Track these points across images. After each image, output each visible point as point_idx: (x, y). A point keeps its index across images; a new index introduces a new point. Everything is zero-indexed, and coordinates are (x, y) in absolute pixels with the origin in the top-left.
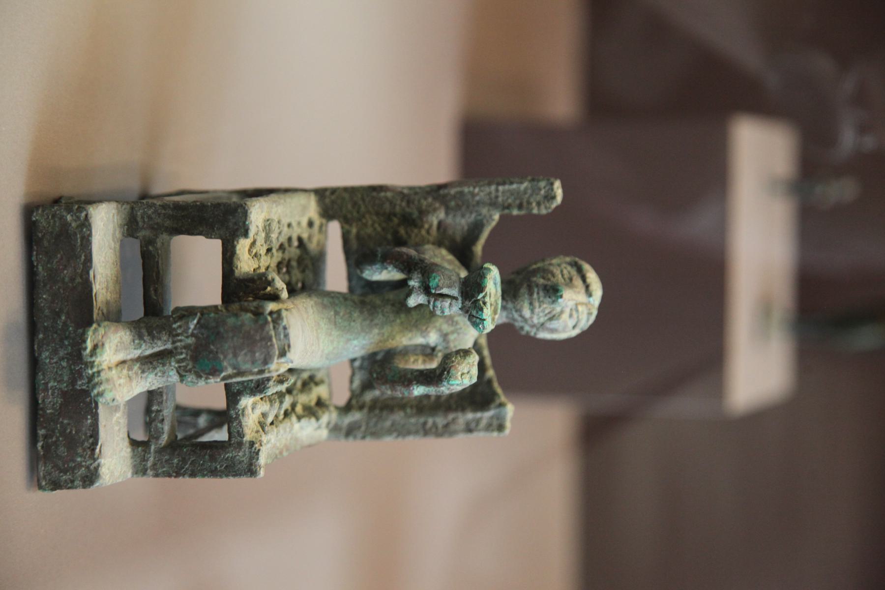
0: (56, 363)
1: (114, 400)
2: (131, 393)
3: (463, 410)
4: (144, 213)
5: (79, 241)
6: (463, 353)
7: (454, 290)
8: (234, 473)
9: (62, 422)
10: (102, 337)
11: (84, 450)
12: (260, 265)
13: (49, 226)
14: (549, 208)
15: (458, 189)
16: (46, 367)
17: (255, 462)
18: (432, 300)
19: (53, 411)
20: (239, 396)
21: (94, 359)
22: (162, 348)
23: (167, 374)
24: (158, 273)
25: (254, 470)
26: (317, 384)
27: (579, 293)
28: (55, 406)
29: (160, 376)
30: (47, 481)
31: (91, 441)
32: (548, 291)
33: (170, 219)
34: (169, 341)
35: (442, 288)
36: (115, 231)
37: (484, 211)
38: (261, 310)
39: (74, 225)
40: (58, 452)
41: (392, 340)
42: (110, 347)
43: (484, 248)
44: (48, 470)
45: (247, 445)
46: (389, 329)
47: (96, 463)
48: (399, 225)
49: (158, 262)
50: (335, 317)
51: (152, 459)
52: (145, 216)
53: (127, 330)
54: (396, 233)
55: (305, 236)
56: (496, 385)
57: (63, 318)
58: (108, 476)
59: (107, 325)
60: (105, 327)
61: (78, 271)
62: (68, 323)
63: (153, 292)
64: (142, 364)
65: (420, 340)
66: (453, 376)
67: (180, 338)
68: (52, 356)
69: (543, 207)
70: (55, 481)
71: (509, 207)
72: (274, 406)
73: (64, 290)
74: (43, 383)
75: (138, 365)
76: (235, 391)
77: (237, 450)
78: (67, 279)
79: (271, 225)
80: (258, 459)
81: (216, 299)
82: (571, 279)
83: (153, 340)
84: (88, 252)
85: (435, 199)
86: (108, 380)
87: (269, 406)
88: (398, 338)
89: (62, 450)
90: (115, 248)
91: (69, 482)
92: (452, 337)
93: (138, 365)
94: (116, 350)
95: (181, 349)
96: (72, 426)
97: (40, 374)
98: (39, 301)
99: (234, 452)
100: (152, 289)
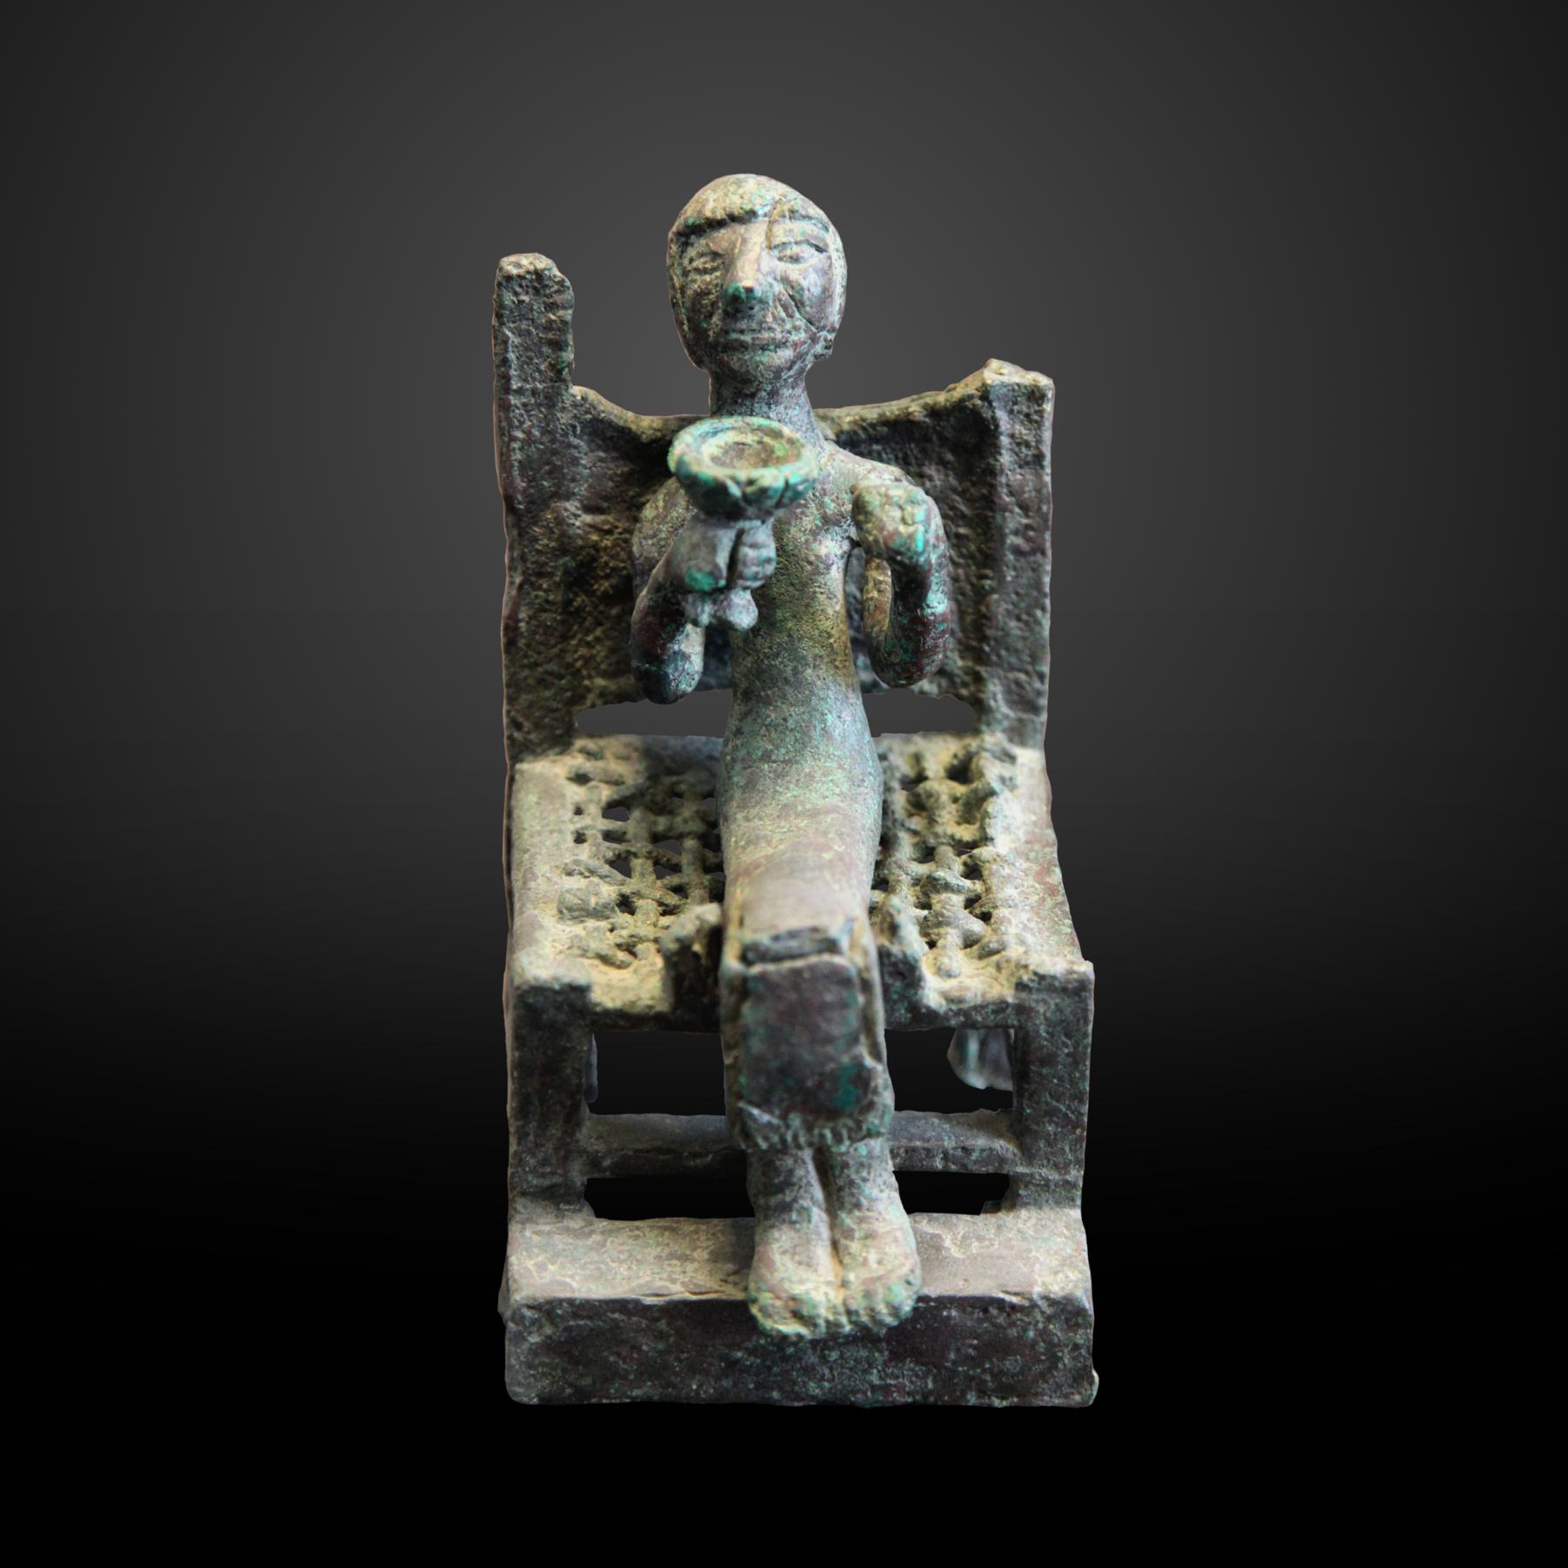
0: (831, 1369)
1: (909, 1283)
3: (992, 472)
4: (533, 1171)
5: (582, 1323)
6: (859, 513)
7: (720, 540)
8: (1082, 1021)
9: (954, 1363)
10: (778, 1298)
11: (1013, 1324)
12: (652, 937)
13: (550, 1374)
14: (561, 283)
15: (516, 473)
16: (840, 1387)
17: (1060, 982)
18: (740, 582)
19: (930, 1378)
20: (920, 1009)
21: (821, 1322)
22: (811, 1167)
23: (865, 1160)
25: (1075, 984)
27: (744, 241)
28: (920, 1373)
29: (869, 1173)
30: (1072, 1390)
31: (994, 1311)
32: (737, 311)
33: (548, 1126)
34: (797, 1154)
35: (716, 566)
36: (567, 1230)
37: (564, 418)
38: (737, 983)
39: (548, 1330)
41: (830, 636)
42: (801, 1282)
43: (640, 410)
45: (1024, 995)
46: (806, 644)
47: (1040, 1303)
48: (591, 593)
50: (774, 762)
51: (1044, 1172)
52: (541, 1170)
53: (769, 1235)
54: (606, 599)
55: (606, 793)
56: (941, 398)
57: (739, 1354)
58: (1070, 1274)
59: (756, 1283)
60: (759, 1290)
61: (644, 1326)
62: (750, 1346)
63: (698, 1161)
64: (842, 1206)
65: (835, 575)
66: (906, 544)
67: (789, 1138)
68: (818, 1376)
69: (558, 298)
70: (1074, 1378)
71: (557, 370)
72: (948, 917)
73: (683, 1352)
74: (873, 1392)
75: (843, 1215)
76: (909, 1015)
77: (1033, 1014)
78: (661, 1346)
79: (569, 905)
80: (1054, 978)
82: (715, 255)
83: (793, 1185)
84: (604, 1307)
85: (535, 521)
86: (868, 1295)
87: (949, 930)
88: (826, 625)
89: (1011, 1364)
90: (603, 1233)
91: (1076, 1353)
92: (831, 508)
93: (843, 1215)
94: (809, 1265)
96: (963, 1345)
97: (853, 1399)
98: (703, 1396)
99: (1038, 1022)
100: (692, 1163)
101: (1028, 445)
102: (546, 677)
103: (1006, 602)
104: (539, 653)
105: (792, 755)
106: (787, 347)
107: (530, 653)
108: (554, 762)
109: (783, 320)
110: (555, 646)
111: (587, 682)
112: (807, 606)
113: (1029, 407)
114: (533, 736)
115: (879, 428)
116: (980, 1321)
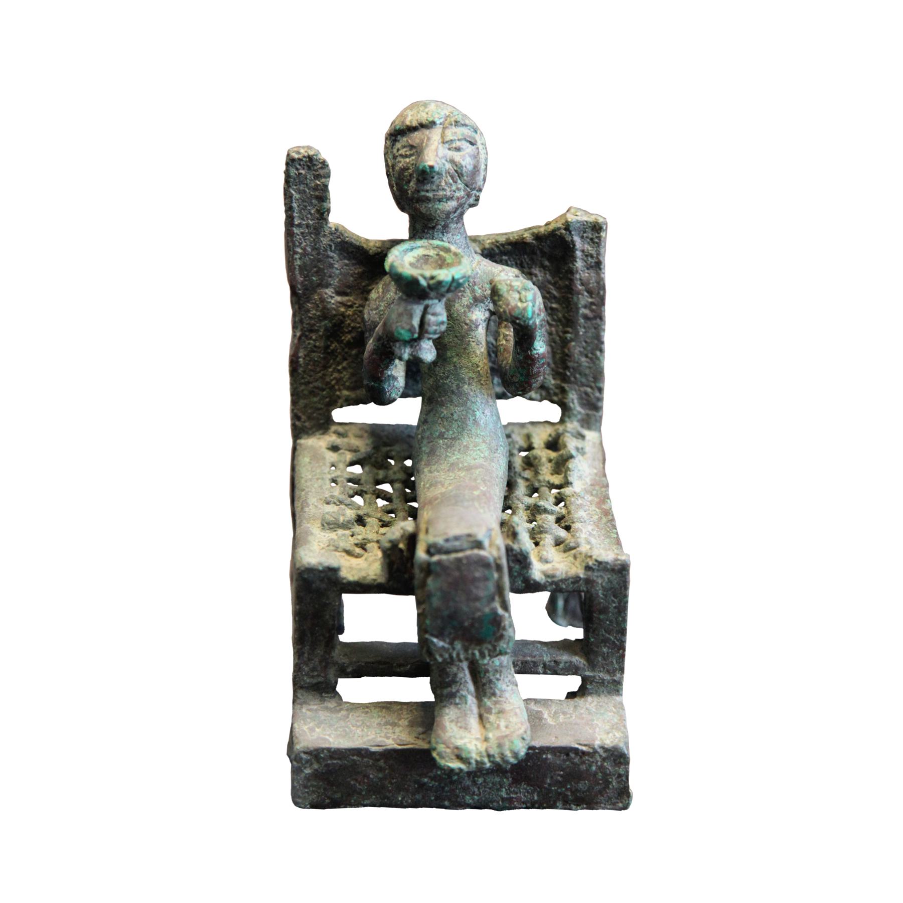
0: (479, 788)
1: (523, 739)
2: (518, 711)
3: (571, 272)
4: (307, 675)
5: (335, 762)
6: (495, 296)
7: (415, 311)
8: (623, 588)
9: (550, 785)
10: (448, 747)
11: (583, 763)
12: (375, 540)
13: (317, 792)
15: (297, 272)
17: (611, 566)
19: (536, 794)
20: (530, 581)
21: (473, 761)
22: (467, 672)
23: (498, 668)
25: (619, 567)
28: (530, 791)
29: (500, 676)
30: (618, 801)
31: (572, 755)
32: (425, 179)
33: (316, 648)
34: (459, 665)
35: (412, 326)
36: (327, 708)
37: (325, 241)
38: (425, 566)
39: (316, 766)
40: (585, 790)
41: (478, 366)
42: (461, 738)
45: (590, 573)
46: (464, 371)
47: (599, 750)
48: (340, 342)
49: (366, 663)
50: (446, 439)
51: (601, 675)
52: (311, 674)
53: (443, 711)
54: (349, 345)
57: (426, 780)
58: (616, 734)
59: (435, 739)
60: (437, 743)
61: (371, 763)
62: (432, 775)
64: (485, 695)
65: (481, 331)
67: (454, 655)
68: (471, 793)
70: (619, 794)
72: (546, 528)
73: (393, 779)
74: (502, 802)
75: (486, 700)
76: (523, 585)
78: (380, 775)
79: (328, 521)
80: (607, 563)
81: (410, 601)
82: (412, 147)
83: (457, 682)
84: (348, 753)
85: (308, 300)
86: (500, 746)
87: (547, 535)
88: (476, 360)
89: (582, 786)
91: (620, 779)
92: (479, 292)
93: (486, 700)
94: (466, 729)
96: (555, 774)
99: (598, 589)
100: (398, 670)
102: (314, 390)
103: (580, 347)
104: (311, 376)
105: (456, 435)
106: (453, 200)
108: (319, 439)
109: (451, 185)
110: (320, 372)
111: (338, 393)
112: (465, 349)
113: (592, 235)
114: (307, 424)
115: (506, 247)
116: (564, 761)
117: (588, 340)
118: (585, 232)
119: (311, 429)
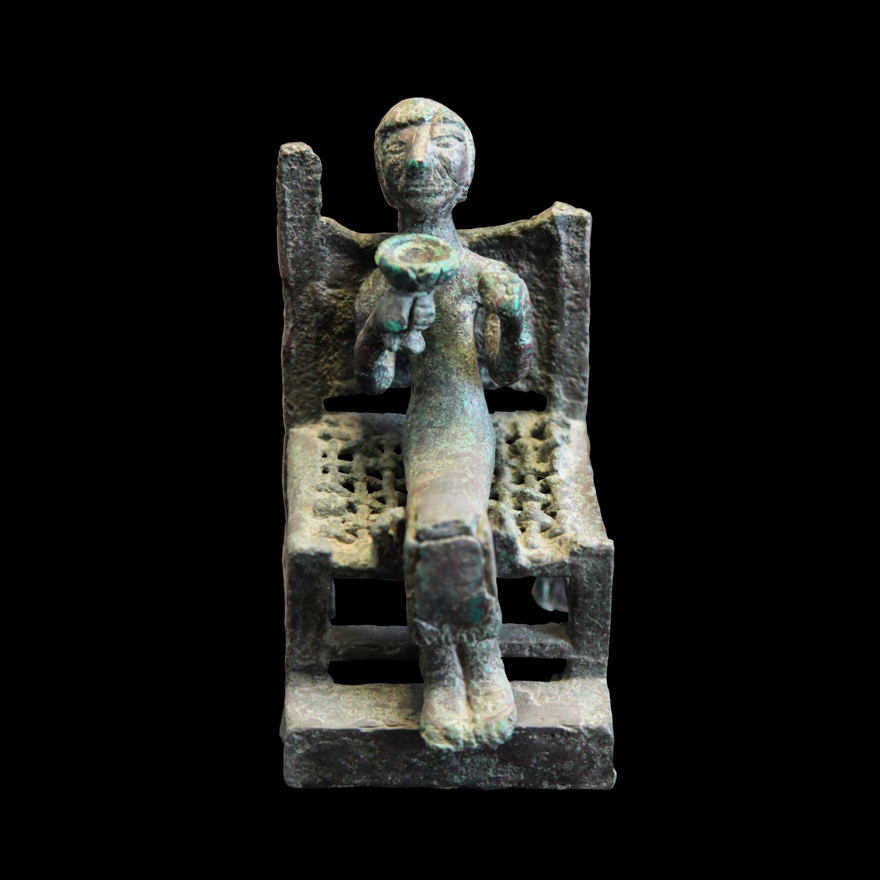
0: (466, 768)
1: (510, 720)
3: (557, 265)
4: (299, 657)
5: (327, 742)
6: (482, 288)
7: (404, 303)
8: (607, 573)
9: (536, 765)
10: (437, 728)
11: (569, 743)
12: (366, 526)
13: (309, 771)
14: (315, 159)
15: (289, 265)
16: (471, 778)
17: (595, 551)
19: (522, 773)
20: (516, 566)
21: (461, 742)
22: (455, 655)
23: (485, 651)
24: (370, 646)
25: (604, 552)
26: (517, 436)
27: (418, 135)
28: (516, 771)
29: (488, 658)
30: (602, 780)
31: (558, 736)
33: (308, 632)
34: (447, 648)
35: (402, 318)
36: (318, 690)
37: (317, 235)
38: (414, 552)
39: (308, 747)
41: (466, 357)
42: (450, 719)
43: (360, 230)
44: (589, 780)
45: (575, 558)
46: (452, 361)
47: (584, 731)
48: (332, 333)
50: (434, 428)
51: (586, 658)
52: (303, 657)
53: (432, 693)
54: (340, 336)
57: (415, 760)
58: (600, 715)
59: (424, 720)
60: (426, 724)
61: (361, 744)
62: (421, 755)
63: (392, 652)
64: (472, 677)
65: (469, 323)
67: (443, 639)
68: (459, 772)
69: (313, 167)
70: (603, 773)
73: (383, 759)
74: (490, 781)
75: (473, 682)
76: (510, 570)
78: (371, 756)
79: (320, 508)
80: (591, 549)
82: (401, 143)
83: (445, 665)
84: (339, 733)
85: (300, 292)
86: (487, 727)
87: (533, 522)
88: (464, 351)
89: (567, 766)
90: (338, 692)
91: (604, 760)
92: (466, 285)
93: (473, 682)
94: (454, 710)
95: (456, 637)
96: (541, 755)
97: (479, 785)
98: (395, 783)
100: (388, 653)
101: (577, 250)
102: (306, 380)
103: (565, 338)
104: (303, 367)
105: (444, 423)
106: (442, 195)
107: (297, 366)
108: (311, 427)
109: (440, 180)
110: (311, 363)
111: (329, 383)
112: (453, 340)
113: (577, 229)
114: (299, 413)
115: (493, 240)
116: (550, 741)
117: (573, 332)
118: (570, 226)
119: (303, 418)
